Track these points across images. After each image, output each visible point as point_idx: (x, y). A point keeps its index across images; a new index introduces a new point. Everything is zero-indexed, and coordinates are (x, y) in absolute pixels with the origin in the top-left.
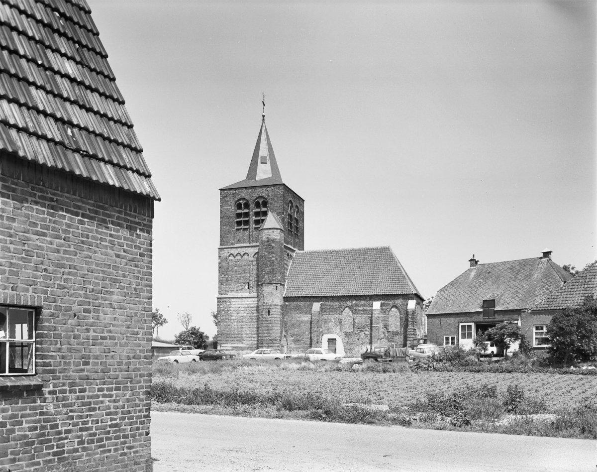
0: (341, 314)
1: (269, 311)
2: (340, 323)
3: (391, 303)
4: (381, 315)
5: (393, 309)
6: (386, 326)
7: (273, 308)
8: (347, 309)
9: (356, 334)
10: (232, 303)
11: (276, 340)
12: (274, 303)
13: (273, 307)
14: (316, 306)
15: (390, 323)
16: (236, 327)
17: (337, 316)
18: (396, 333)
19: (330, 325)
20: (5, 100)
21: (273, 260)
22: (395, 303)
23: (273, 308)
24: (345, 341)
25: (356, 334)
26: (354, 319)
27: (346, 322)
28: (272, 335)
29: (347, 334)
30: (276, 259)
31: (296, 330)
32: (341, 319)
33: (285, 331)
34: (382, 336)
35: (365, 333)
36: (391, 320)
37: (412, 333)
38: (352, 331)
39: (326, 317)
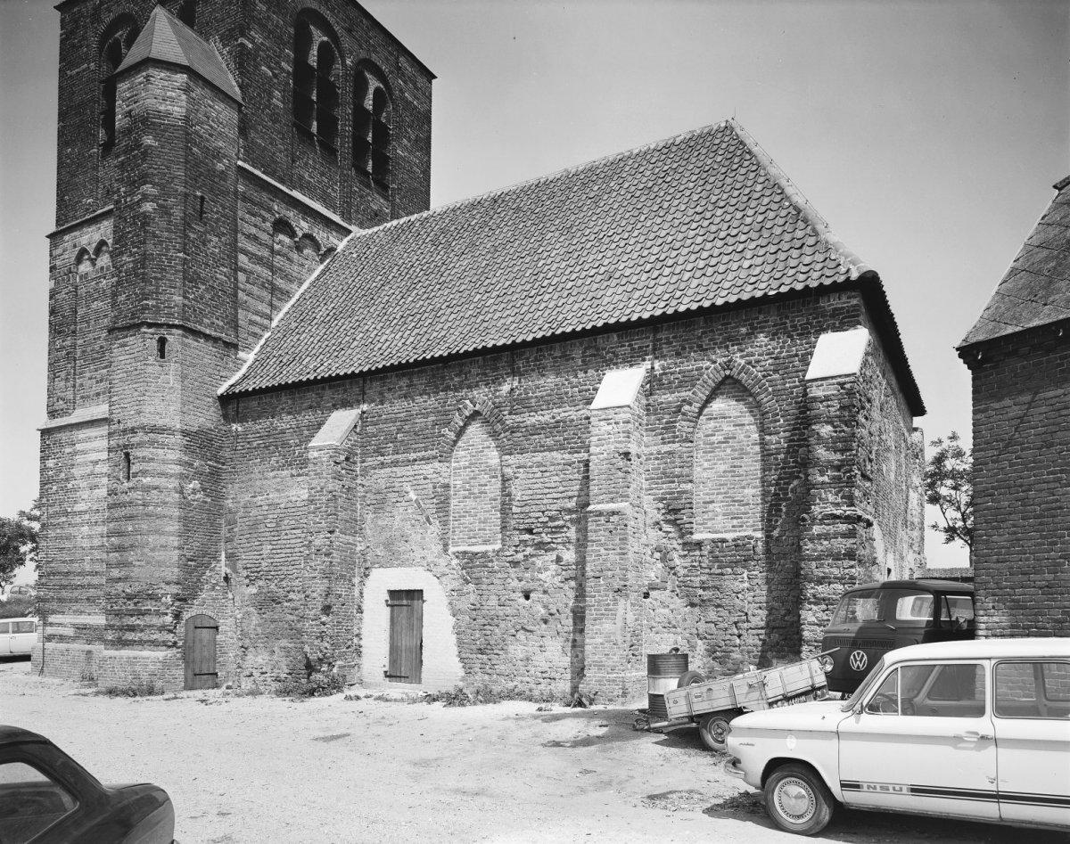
0: (444, 457)
1: (127, 455)
2: (443, 506)
3: (709, 366)
4: (644, 445)
5: (718, 405)
6: (675, 513)
7: (140, 445)
8: (475, 431)
9: (515, 564)
10: (79, 447)
11: (153, 597)
12: (145, 420)
13: (139, 437)
14: (339, 424)
15: (700, 495)
16: (86, 543)
17: (428, 469)
18: (732, 555)
19: (400, 518)
20: (900, 600)
21: (145, 215)
22: (728, 365)
23: (140, 445)
24: (464, 604)
25: (515, 564)
26: (505, 480)
27: (470, 503)
28: (136, 572)
29: (470, 561)
30: (164, 211)
31: (267, 549)
32: (447, 486)
33: (230, 557)
34: (654, 572)
35: (559, 560)
36: (708, 472)
37: (842, 545)
38: (498, 546)
39: (380, 478)
